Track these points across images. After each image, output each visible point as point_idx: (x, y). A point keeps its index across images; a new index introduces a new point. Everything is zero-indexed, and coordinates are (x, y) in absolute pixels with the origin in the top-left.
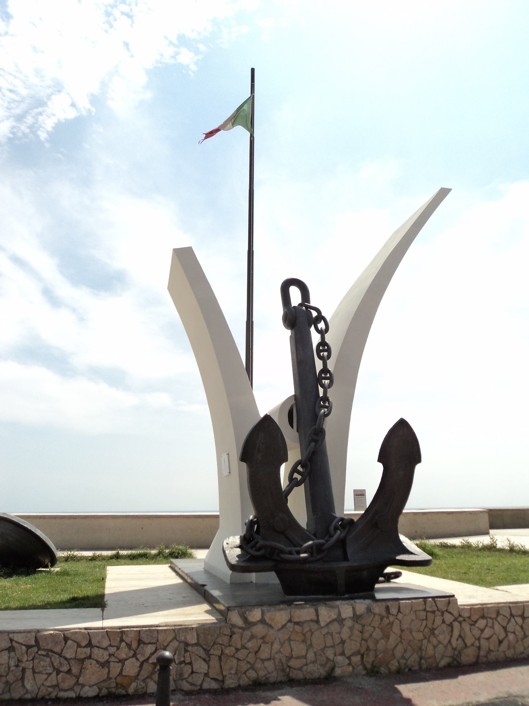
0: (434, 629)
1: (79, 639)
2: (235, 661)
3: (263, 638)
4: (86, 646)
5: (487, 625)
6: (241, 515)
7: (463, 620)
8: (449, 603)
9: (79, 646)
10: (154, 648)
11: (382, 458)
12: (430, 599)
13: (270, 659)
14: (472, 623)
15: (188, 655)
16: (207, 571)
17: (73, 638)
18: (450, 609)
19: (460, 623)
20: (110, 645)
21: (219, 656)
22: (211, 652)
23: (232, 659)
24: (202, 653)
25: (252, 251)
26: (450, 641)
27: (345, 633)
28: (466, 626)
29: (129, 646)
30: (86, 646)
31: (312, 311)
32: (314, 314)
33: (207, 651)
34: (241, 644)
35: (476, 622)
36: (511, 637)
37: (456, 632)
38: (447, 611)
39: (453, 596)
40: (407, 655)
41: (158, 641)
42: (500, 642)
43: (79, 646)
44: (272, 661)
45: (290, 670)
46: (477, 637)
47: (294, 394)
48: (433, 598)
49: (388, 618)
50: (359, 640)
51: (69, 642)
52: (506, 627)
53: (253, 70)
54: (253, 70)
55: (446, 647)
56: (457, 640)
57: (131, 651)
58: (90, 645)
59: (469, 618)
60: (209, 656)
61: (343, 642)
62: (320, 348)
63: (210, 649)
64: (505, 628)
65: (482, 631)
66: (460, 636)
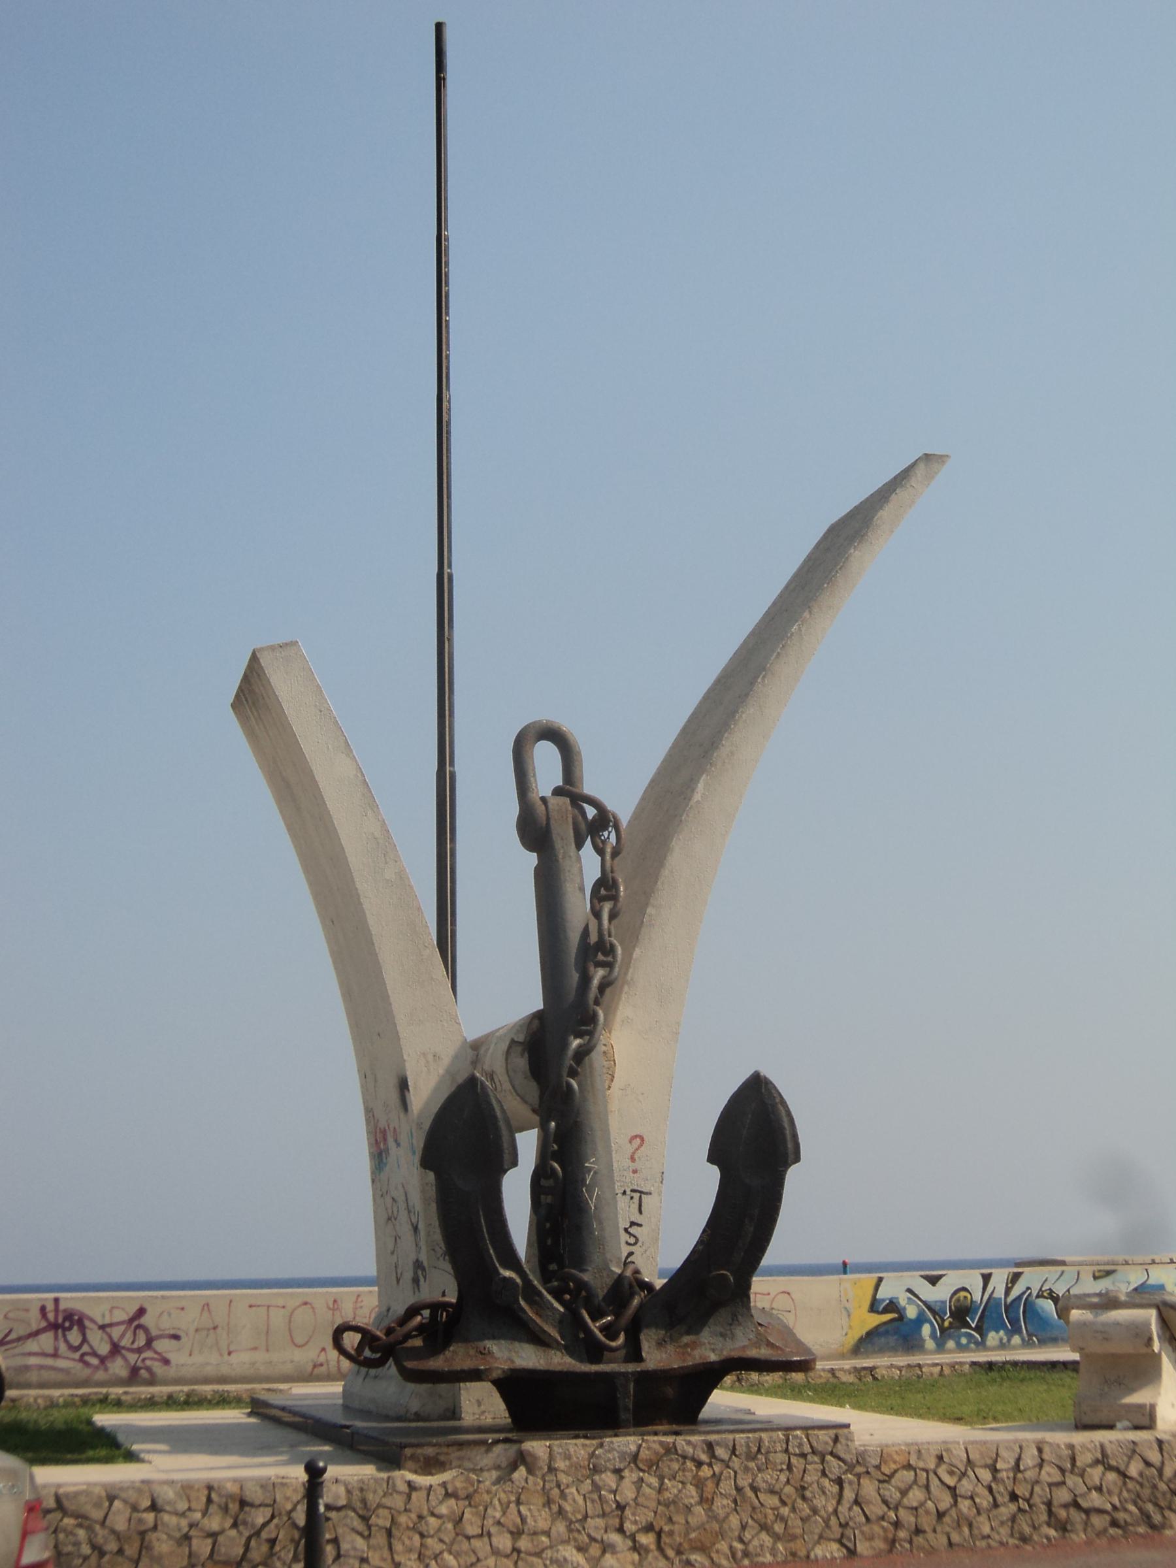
0: (803, 1488)
1: (132, 1496)
2: (417, 1538)
3: (468, 1497)
4: (147, 1510)
5: (915, 1482)
6: (731, 656)
7: (864, 1473)
8: (836, 1440)
9: (135, 1508)
10: (269, 1515)
11: (714, 1157)
12: (798, 1432)
13: (482, 1535)
14: (882, 1478)
15: (331, 1526)
16: (346, 1407)
17: (123, 1495)
18: (840, 1449)
19: (859, 1476)
20: (190, 1509)
21: (386, 1529)
22: (373, 1520)
23: (411, 1533)
24: (357, 1524)
25: (448, 964)
26: (836, 1511)
27: (628, 1492)
28: (869, 1488)
29: (225, 1509)
30: (147, 1510)
31: (585, 805)
32: (591, 812)
33: (365, 1519)
34: (429, 1509)
35: (891, 1476)
36: (965, 1505)
37: (849, 1495)
38: (831, 1454)
39: (848, 1426)
40: (747, 1536)
41: (275, 1501)
42: (940, 1515)
43: (135, 1508)
44: (486, 1539)
45: (518, 1556)
46: (893, 1504)
47: (538, 1005)
48: (805, 1429)
49: (710, 1465)
50: (653, 1504)
51: (117, 1503)
52: (955, 1488)
53: (439, 27)
54: (439, 27)
55: (827, 1522)
56: (850, 1509)
57: (228, 1518)
58: (154, 1507)
59: (878, 1467)
60: (369, 1527)
61: (621, 1507)
62: (600, 891)
63: (371, 1516)
64: (953, 1490)
65: (904, 1493)
66: (856, 1502)
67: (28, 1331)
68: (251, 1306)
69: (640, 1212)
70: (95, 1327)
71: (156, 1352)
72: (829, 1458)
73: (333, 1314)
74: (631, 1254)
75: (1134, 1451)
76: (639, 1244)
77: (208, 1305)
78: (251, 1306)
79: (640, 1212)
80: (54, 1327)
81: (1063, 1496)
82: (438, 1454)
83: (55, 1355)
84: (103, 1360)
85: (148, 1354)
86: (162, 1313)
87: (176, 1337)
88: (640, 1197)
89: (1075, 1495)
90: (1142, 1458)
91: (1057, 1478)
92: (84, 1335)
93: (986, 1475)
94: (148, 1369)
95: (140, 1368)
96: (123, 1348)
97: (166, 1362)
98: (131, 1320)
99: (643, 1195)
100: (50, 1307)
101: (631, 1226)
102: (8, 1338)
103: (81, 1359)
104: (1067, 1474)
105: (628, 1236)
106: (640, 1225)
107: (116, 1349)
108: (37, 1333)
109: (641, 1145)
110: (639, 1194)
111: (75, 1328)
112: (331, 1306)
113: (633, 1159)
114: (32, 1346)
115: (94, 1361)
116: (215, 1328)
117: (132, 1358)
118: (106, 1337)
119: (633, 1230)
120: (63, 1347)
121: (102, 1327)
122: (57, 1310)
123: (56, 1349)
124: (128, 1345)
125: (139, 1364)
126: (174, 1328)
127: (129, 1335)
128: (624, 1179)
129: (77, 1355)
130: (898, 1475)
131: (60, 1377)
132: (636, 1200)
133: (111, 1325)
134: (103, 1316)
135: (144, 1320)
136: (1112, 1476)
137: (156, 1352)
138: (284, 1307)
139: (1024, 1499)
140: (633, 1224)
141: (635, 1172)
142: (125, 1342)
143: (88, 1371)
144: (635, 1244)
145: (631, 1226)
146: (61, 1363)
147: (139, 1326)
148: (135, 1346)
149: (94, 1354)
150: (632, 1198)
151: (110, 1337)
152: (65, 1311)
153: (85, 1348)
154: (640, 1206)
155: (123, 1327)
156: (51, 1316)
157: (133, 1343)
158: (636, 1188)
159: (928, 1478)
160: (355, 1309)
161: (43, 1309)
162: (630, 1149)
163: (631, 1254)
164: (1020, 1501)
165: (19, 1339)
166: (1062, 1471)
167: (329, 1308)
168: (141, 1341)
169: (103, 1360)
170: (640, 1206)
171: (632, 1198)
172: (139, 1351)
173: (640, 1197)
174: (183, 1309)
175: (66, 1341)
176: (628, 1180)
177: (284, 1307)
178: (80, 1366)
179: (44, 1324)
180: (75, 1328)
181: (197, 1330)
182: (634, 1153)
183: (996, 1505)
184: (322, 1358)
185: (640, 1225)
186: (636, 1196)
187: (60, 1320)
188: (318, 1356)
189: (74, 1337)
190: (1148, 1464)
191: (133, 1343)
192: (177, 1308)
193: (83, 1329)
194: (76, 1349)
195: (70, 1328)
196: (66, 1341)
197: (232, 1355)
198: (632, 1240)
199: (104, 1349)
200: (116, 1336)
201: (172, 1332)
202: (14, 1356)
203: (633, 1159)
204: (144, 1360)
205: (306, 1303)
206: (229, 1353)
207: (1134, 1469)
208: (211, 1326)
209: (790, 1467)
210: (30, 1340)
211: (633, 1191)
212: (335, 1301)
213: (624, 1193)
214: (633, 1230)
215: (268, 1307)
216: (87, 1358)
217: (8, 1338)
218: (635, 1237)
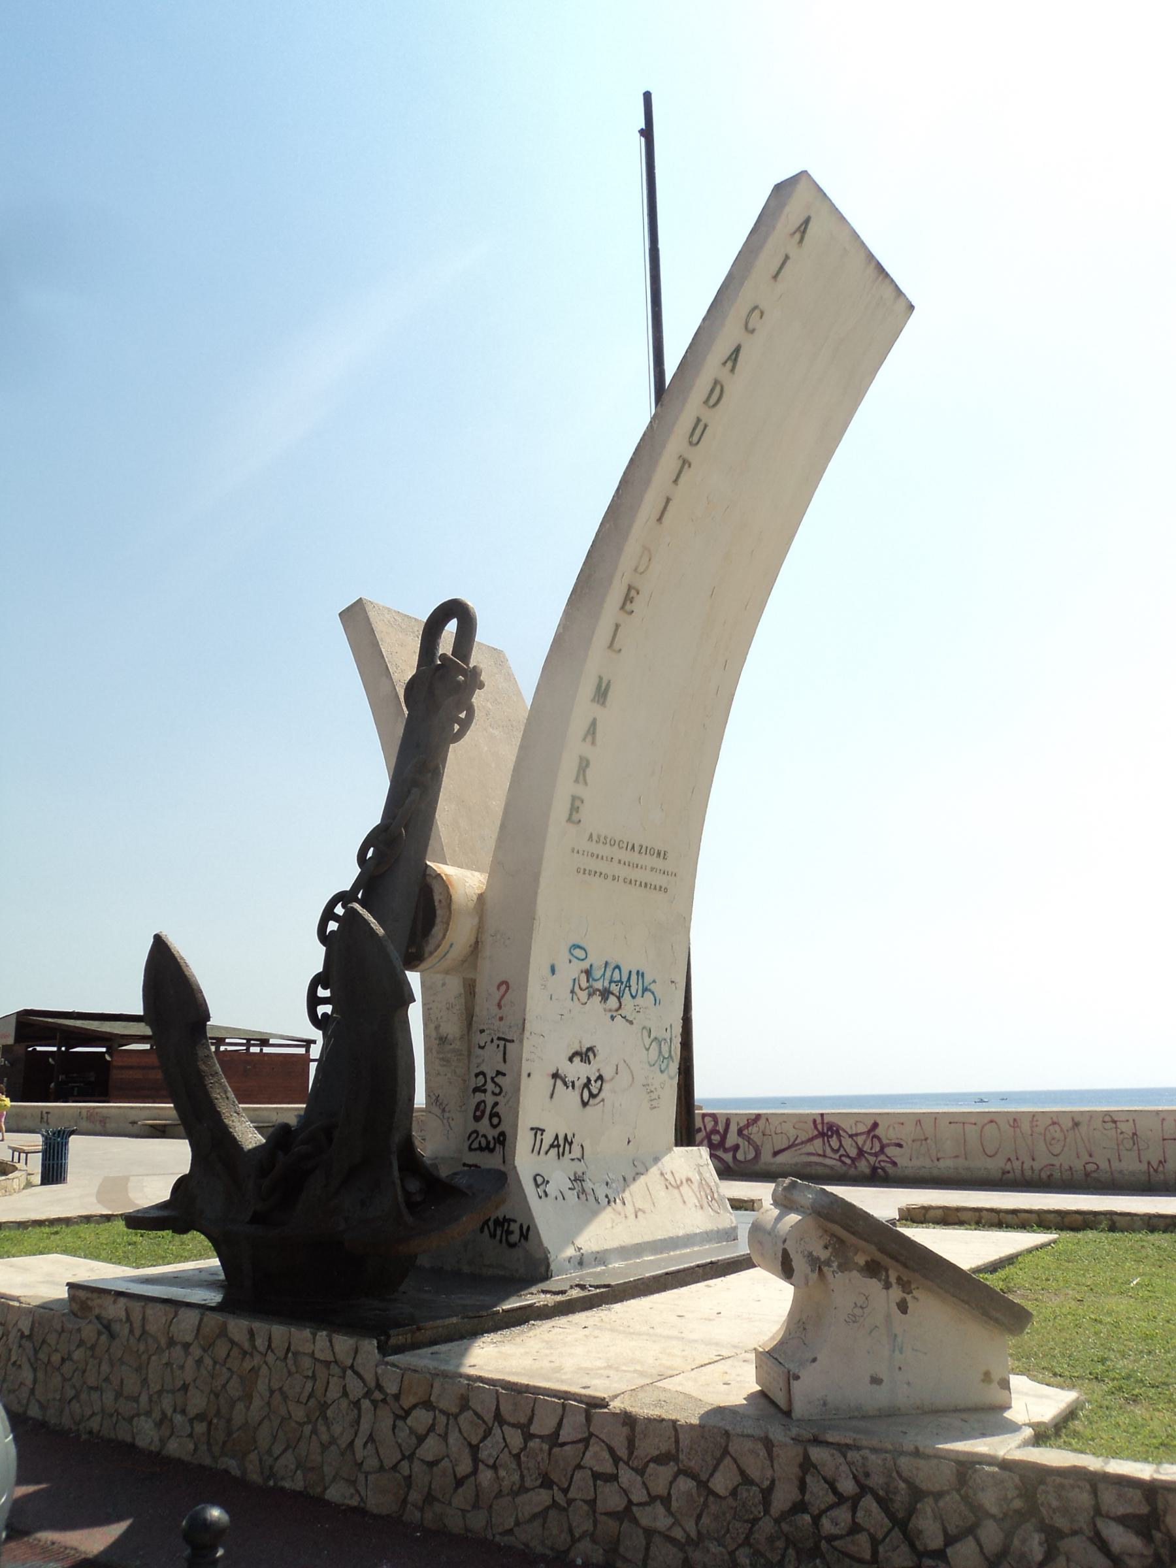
35: (408, 1413)
66: (371, 1438)
67: (807, 1137)
68: (950, 1123)
69: (505, 1061)
70: (847, 1136)
71: (887, 1157)
72: (349, 1372)
73: (1015, 1131)
74: (496, 1104)
75: (726, 1452)
76: (503, 1094)
77: (919, 1121)
78: (950, 1123)
79: (505, 1061)
80: (822, 1135)
81: (611, 1499)
82: (87, 1299)
83: (824, 1156)
84: (853, 1160)
85: (882, 1157)
86: (889, 1126)
87: (900, 1146)
88: (505, 1044)
89: (630, 1502)
90: (738, 1466)
91: (607, 1467)
92: (840, 1141)
93: (515, 1439)
94: (883, 1169)
95: (877, 1168)
96: (866, 1152)
97: (894, 1164)
98: (869, 1132)
99: (507, 1043)
100: (819, 1120)
101: (497, 1075)
102: (796, 1142)
103: (840, 1160)
104: (621, 1464)
105: (493, 1085)
106: (504, 1075)
107: (861, 1152)
108: (811, 1140)
109: (508, 988)
110: (504, 1042)
111: (835, 1136)
112: (1012, 1124)
113: (499, 1006)
114: (809, 1148)
115: (848, 1161)
116: (926, 1139)
117: (872, 1159)
118: (854, 1144)
119: (499, 1080)
120: (828, 1150)
121: (851, 1136)
122: (823, 1123)
123: (824, 1151)
124: (869, 1151)
125: (877, 1165)
126: (898, 1139)
127: (869, 1143)
128: (492, 1027)
129: (837, 1156)
130: (415, 1413)
131: (828, 1171)
132: (501, 1048)
133: (857, 1135)
134: (851, 1128)
135: (878, 1132)
136: (685, 1485)
137: (887, 1157)
138: (975, 1124)
139: (560, 1489)
140: (499, 1073)
141: (501, 1019)
142: (866, 1148)
143: (845, 1168)
144: (500, 1094)
145: (497, 1075)
146: (828, 1162)
147: (875, 1136)
148: (873, 1151)
149: (848, 1156)
150: (498, 1046)
151: (856, 1143)
152: (827, 1123)
153: (842, 1152)
154: (505, 1054)
155: (864, 1137)
156: (820, 1127)
157: (871, 1149)
158: (501, 1035)
159: (447, 1424)
160: (1032, 1127)
161: (815, 1121)
162: (497, 995)
163: (496, 1104)
164: (555, 1488)
165: (802, 1143)
166: (616, 1459)
167: (1010, 1126)
168: (877, 1148)
169: (853, 1160)
170: (505, 1054)
171: (498, 1046)
172: (876, 1155)
173: (505, 1044)
174: (902, 1124)
175: (830, 1145)
176: (496, 1028)
177: (975, 1124)
178: (839, 1163)
179: (816, 1133)
180: (835, 1136)
181: (913, 1141)
182: (500, 1000)
183: (523, 1489)
184: (1008, 1167)
185: (504, 1075)
186: (502, 1043)
187: (825, 1130)
188: (1006, 1165)
189: (834, 1142)
190: (747, 1480)
191: (871, 1149)
192: (899, 1123)
193: (839, 1136)
194: (836, 1151)
195: (831, 1136)
196: (830, 1145)
197: (940, 1160)
198: (497, 1090)
199: (853, 1152)
200: (860, 1143)
201: (897, 1141)
202: (801, 1154)
203: (499, 1006)
204: (879, 1162)
205: (992, 1121)
206: (938, 1160)
207: (721, 1483)
208: (923, 1138)
209: (314, 1377)
210: (808, 1144)
211: (499, 1039)
212: (1015, 1120)
213: (492, 1041)
214: (499, 1080)
215: (964, 1123)
216: (844, 1159)
217: (796, 1142)
218: (500, 1086)
